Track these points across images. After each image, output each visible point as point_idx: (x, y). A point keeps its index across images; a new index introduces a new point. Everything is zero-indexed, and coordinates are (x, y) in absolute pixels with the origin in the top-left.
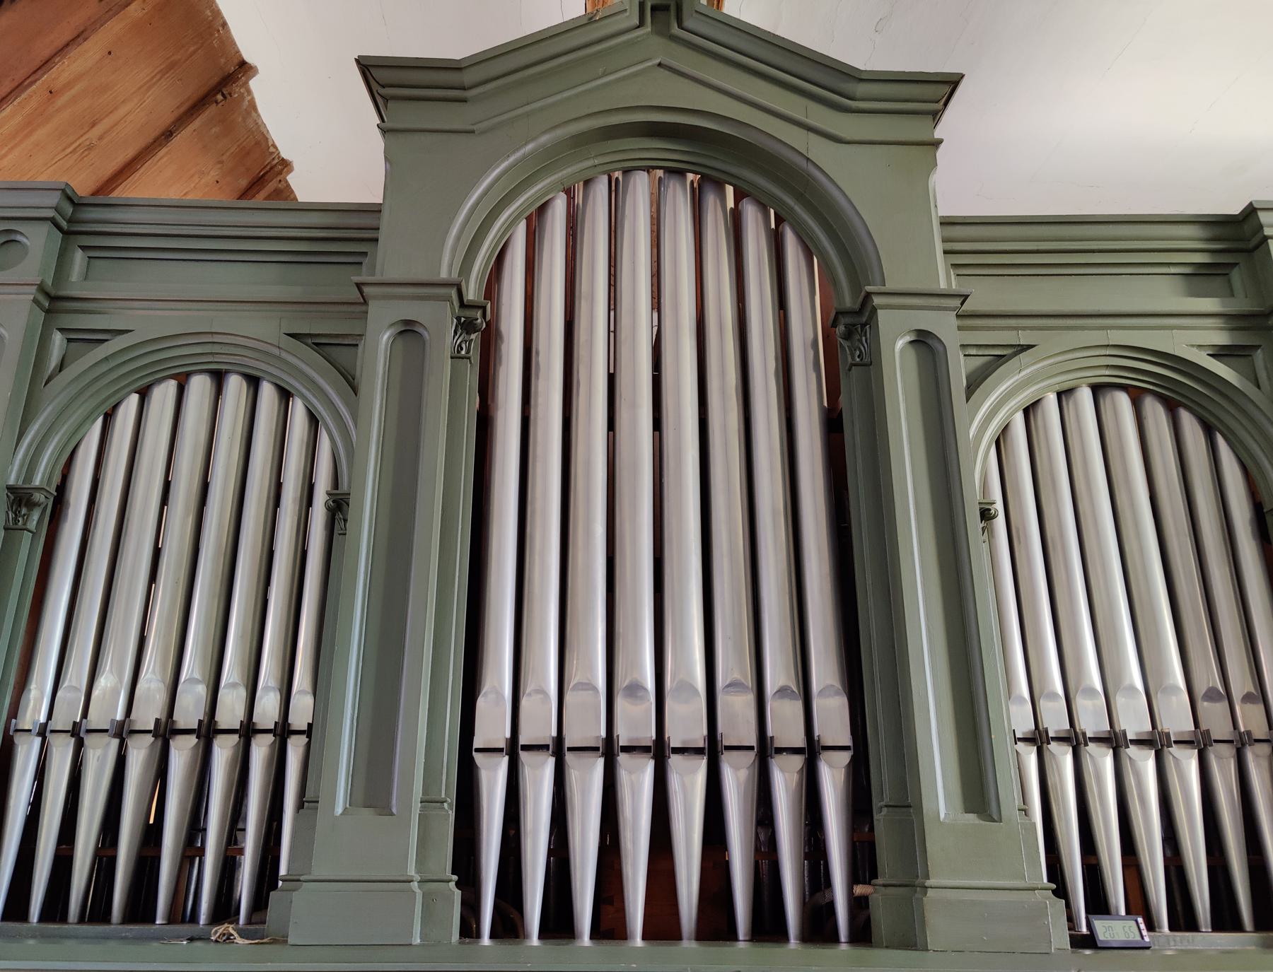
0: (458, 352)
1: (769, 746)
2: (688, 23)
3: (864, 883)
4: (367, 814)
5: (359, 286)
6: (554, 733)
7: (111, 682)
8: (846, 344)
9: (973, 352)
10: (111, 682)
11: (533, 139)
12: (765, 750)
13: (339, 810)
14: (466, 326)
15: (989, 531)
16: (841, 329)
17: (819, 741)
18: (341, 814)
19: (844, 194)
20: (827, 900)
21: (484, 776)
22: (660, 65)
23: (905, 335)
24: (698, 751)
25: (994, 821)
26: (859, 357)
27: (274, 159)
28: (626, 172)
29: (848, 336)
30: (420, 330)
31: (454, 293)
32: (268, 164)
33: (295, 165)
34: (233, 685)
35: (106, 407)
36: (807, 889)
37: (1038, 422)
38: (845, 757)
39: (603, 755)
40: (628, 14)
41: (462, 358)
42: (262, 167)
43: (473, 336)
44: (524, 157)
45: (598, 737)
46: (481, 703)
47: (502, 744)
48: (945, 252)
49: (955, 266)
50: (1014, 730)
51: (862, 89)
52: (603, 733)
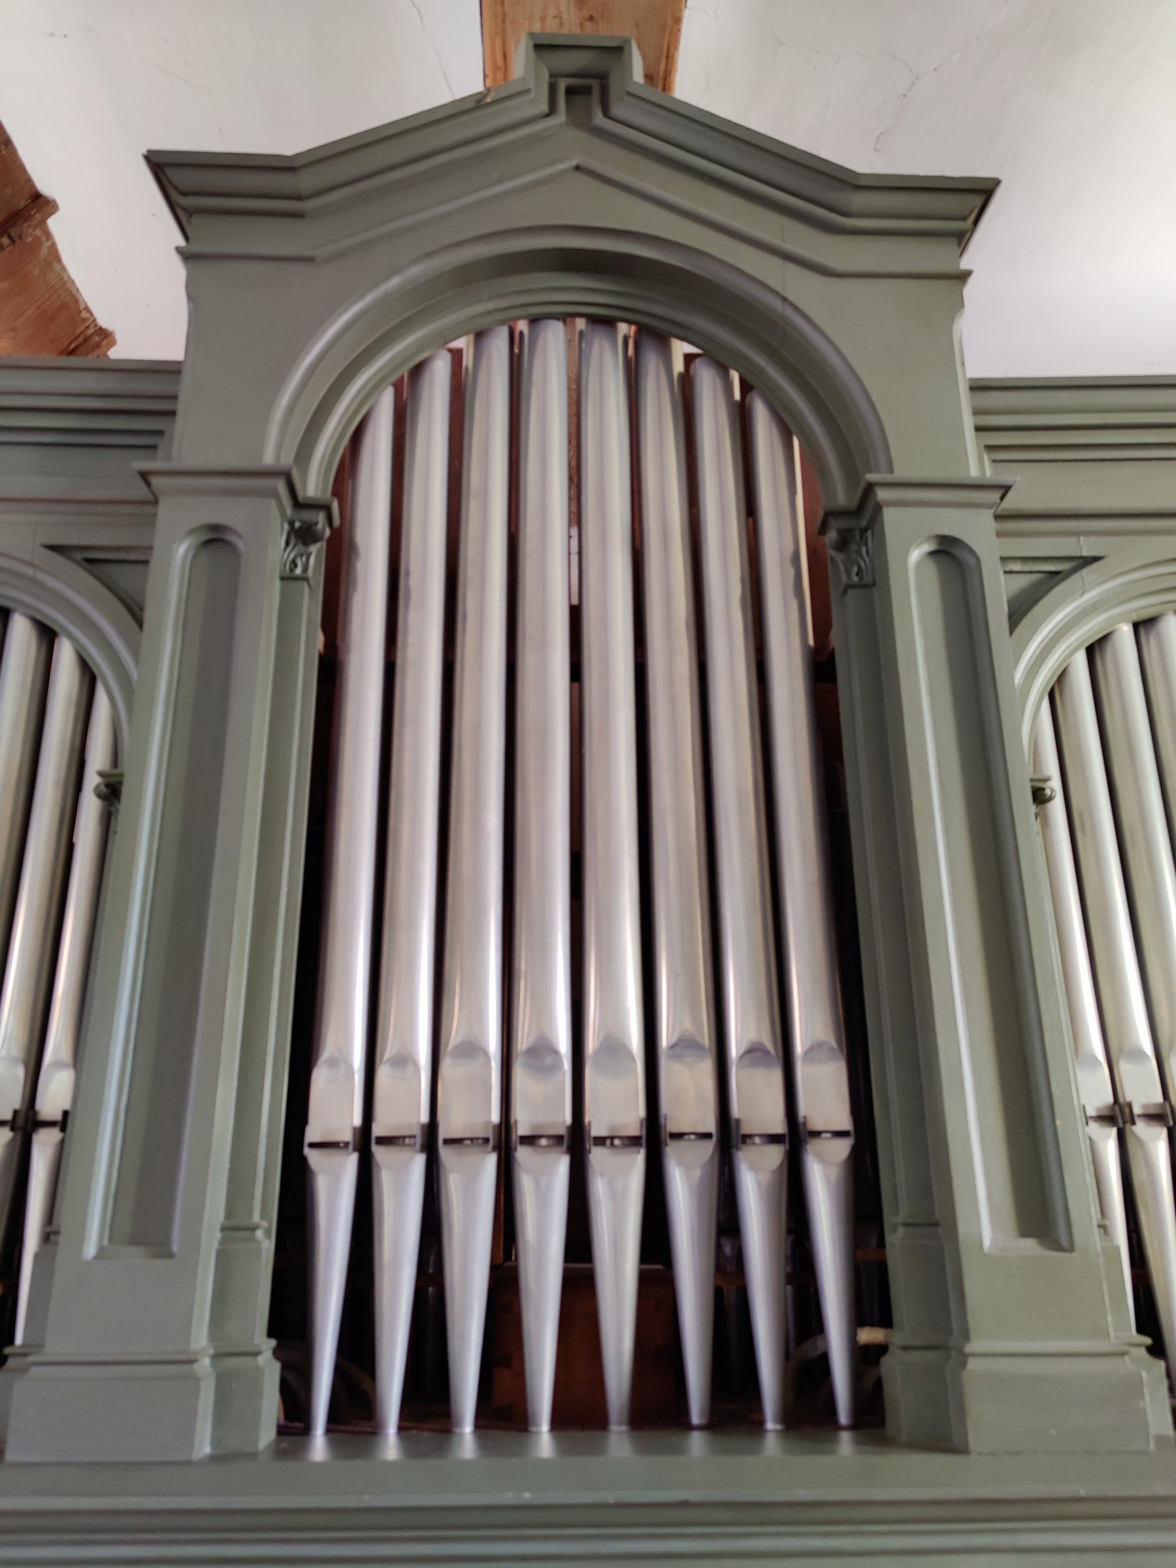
0: (291, 570)
1: (734, 1131)
2: (617, 110)
3: (871, 1324)
4: (134, 1256)
5: (144, 476)
6: (424, 1117)
8: (839, 557)
9: (1017, 567)
11: (397, 271)
13: (90, 1250)
14: (303, 535)
15: (1043, 819)
16: (832, 536)
17: (805, 1124)
18: (96, 1258)
19: (524, 1558)
20: (819, 1352)
21: (322, 1185)
22: (578, 168)
23: (922, 543)
24: (633, 1141)
25: (1061, 1249)
26: (857, 574)
27: (88, 327)
28: (534, 321)
29: (843, 544)
30: (232, 538)
31: (281, 486)
32: (82, 333)
33: (118, 336)
36: (792, 1333)
37: (1106, 665)
38: (843, 1148)
40: (532, 96)
41: (297, 579)
42: (72, 338)
43: (314, 549)
44: (384, 300)
45: (488, 1123)
46: (320, 1078)
47: (346, 1135)
48: (978, 429)
49: (990, 448)
50: (1084, 1107)
51: (859, 200)
52: (495, 1117)
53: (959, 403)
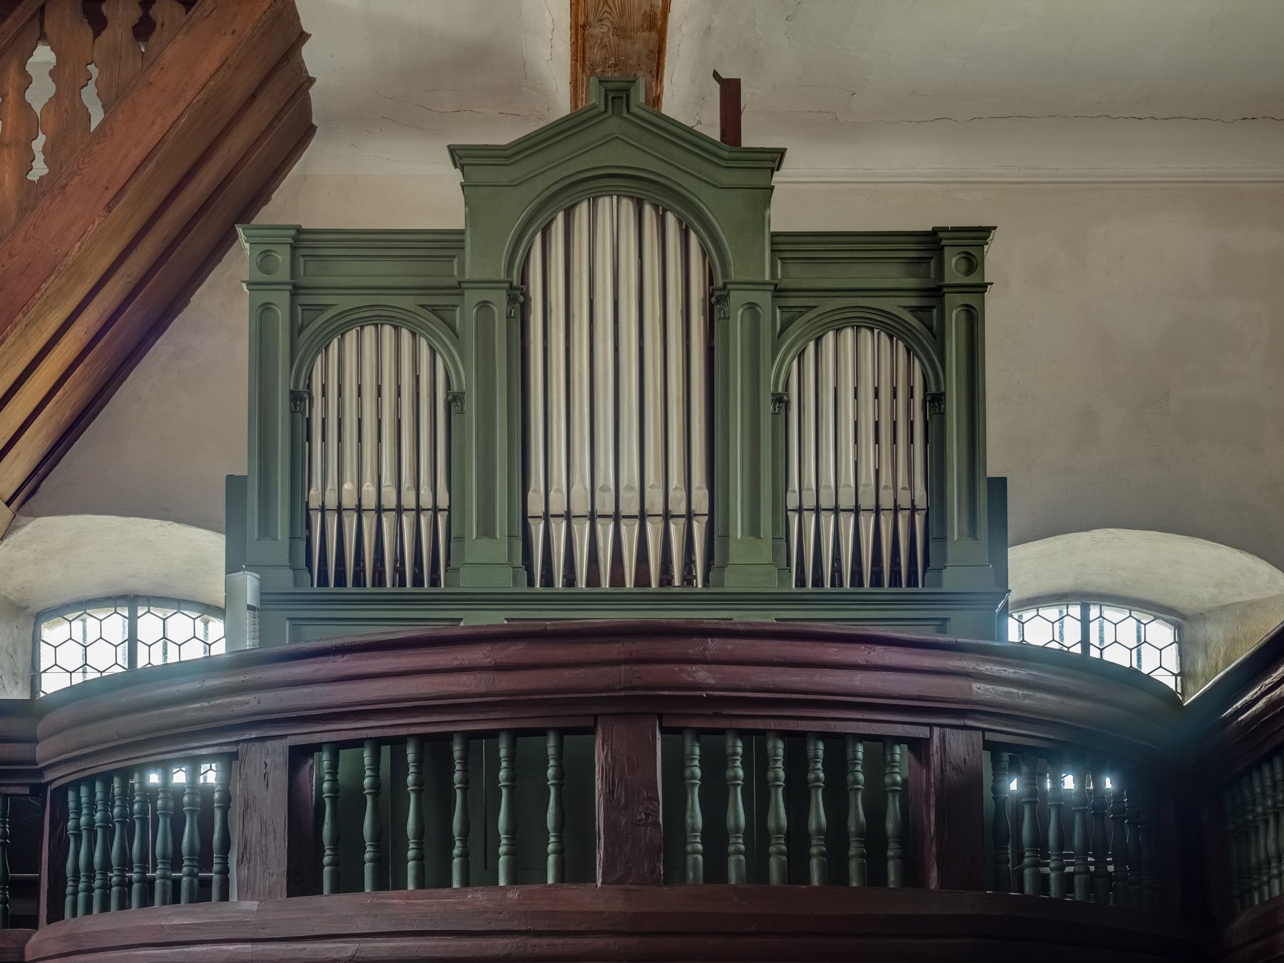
0: (510, 314)
7: (369, 488)
10: (348, 486)
12: (667, 516)
14: (512, 300)
21: (533, 528)
34: (699, 488)
35: (325, 345)
39: (613, 520)
41: (512, 317)
46: (530, 494)
52: (854, 504)
53: (134, 832)
